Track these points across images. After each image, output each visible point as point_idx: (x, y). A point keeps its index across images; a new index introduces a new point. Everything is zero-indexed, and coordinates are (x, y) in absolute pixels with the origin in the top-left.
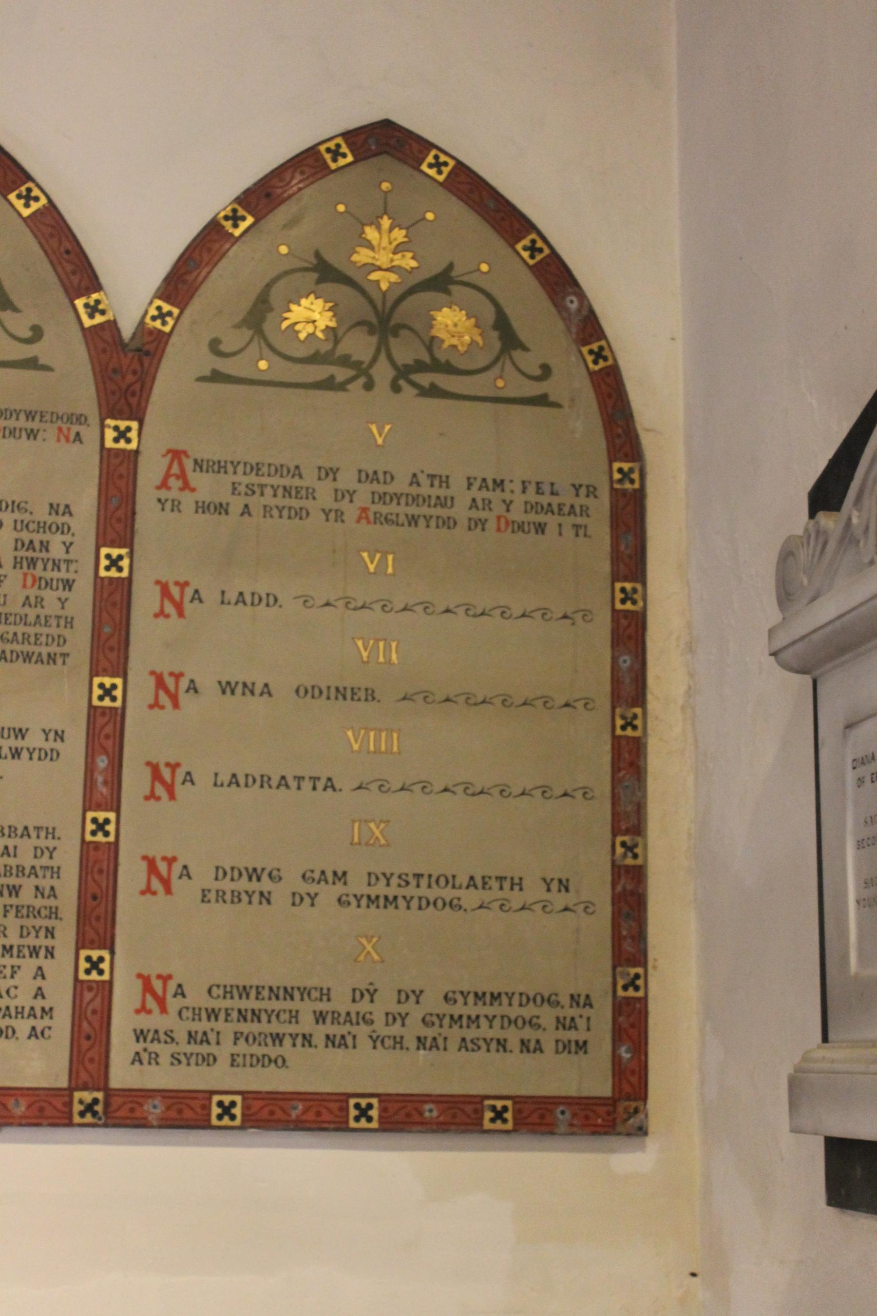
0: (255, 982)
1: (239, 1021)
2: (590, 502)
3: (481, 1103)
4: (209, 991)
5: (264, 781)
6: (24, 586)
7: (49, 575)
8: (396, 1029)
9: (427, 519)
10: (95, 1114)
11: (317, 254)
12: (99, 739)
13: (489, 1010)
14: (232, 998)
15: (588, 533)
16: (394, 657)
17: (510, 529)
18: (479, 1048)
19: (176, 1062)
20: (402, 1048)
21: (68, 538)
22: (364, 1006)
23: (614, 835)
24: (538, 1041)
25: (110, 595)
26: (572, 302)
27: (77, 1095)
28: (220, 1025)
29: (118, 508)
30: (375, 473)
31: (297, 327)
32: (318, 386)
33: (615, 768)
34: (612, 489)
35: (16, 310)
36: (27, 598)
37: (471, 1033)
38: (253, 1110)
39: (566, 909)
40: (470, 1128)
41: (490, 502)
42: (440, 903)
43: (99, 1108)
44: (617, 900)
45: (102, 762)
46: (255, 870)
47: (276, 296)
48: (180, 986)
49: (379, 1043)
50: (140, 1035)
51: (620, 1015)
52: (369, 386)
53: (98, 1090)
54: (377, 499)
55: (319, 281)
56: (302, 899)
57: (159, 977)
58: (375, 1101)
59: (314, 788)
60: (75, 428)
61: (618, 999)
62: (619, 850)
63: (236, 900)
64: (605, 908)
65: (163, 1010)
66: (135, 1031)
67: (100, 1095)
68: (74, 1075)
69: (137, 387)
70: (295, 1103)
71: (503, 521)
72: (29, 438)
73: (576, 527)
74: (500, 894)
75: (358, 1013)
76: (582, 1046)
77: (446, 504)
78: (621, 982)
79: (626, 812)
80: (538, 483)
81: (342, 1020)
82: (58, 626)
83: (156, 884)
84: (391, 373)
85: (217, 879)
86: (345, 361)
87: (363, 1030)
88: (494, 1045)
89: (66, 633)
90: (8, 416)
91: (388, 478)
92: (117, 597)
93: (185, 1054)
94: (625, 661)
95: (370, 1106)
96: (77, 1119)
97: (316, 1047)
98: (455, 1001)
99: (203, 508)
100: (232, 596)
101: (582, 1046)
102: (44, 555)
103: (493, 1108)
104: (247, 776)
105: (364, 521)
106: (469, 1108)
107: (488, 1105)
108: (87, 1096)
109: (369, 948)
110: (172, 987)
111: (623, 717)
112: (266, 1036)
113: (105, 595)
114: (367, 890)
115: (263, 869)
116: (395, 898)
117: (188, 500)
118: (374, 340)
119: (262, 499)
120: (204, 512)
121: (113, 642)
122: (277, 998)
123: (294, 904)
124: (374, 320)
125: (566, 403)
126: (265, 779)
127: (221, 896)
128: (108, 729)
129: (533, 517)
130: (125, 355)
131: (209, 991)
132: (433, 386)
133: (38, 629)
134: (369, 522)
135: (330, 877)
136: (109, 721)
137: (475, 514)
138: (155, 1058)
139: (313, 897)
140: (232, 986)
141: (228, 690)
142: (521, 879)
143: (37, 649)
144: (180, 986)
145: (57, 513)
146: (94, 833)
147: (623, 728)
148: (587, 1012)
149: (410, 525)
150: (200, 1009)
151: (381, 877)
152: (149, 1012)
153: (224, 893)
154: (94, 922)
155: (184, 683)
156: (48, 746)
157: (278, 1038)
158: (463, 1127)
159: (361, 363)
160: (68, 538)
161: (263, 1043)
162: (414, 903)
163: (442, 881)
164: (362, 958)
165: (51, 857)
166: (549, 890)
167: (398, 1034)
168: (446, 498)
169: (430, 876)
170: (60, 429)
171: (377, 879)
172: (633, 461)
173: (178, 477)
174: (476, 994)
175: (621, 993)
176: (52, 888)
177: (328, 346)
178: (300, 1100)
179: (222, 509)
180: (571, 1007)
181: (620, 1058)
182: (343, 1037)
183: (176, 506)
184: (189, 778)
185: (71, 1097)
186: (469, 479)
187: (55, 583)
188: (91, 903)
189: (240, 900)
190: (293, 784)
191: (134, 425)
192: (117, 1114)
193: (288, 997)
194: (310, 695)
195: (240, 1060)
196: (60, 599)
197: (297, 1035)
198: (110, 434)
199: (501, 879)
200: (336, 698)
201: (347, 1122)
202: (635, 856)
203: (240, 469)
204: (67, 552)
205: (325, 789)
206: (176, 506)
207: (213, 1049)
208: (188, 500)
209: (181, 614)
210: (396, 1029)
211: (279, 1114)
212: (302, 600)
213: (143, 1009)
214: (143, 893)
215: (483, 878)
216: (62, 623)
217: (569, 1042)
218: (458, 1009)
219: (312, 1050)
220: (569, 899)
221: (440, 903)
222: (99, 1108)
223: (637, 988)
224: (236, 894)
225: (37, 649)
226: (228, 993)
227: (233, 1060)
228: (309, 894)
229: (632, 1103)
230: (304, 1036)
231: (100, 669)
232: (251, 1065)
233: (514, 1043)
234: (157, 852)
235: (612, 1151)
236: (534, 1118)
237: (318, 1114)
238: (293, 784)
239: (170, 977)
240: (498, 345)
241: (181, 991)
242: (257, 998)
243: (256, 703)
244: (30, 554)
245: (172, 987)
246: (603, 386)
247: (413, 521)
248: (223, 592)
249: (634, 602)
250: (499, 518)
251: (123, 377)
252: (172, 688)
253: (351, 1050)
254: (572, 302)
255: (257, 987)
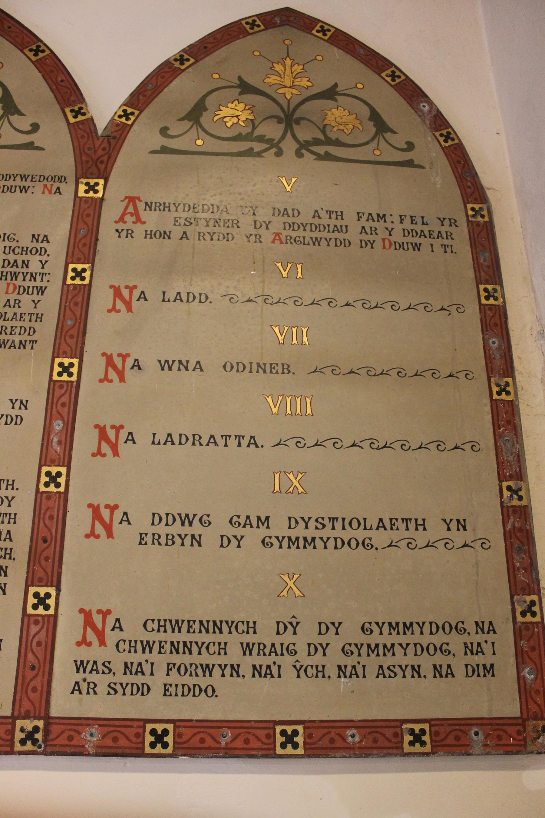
0: (187, 618)
1: (171, 652)
2: (453, 229)
3: (401, 726)
4: (145, 625)
5: (196, 439)
6: (7, 292)
7: (27, 284)
8: (318, 659)
9: (328, 241)
10: (35, 742)
11: (240, 78)
12: (56, 408)
13: (403, 639)
14: (165, 631)
15: (454, 250)
16: (305, 339)
17: (393, 247)
18: (396, 674)
19: (112, 692)
20: (324, 677)
21: (44, 258)
22: (288, 638)
23: (501, 481)
24: (449, 666)
25: (73, 297)
26: (424, 106)
27: (19, 723)
28: (154, 657)
29: (85, 237)
30: (286, 210)
31: (225, 120)
32: (240, 154)
33: (496, 426)
34: (468, 221)
35: (21, 114)
36: (8, 300)
37: (387, 661)
38: (185, 738)
39: (465, 545)
40: (391, 751)
41: (376, 229)
42: (353, 544)
43: (39, 736)
44: (508, 536)
45: (58, 426)
46: (187, 516)
47: (210, 101)
48: (118, 620)
49: (302, 673)
50: (80, 666)
51: (521, 640)
52: (279, 153)
53: (39, 718)
54: (287, 227)
55: (240, 94)
56: (229, 541)
57: (99, 612)
58: (300, 728)
59: (239, 445)
60: (56, 185)
61: (518, 625)
62: (506, 493)
63: (170, 542)
64: (499, 544)
65: (102, 642)
66: (76, 661)
67: (40, 724)
68: (17, 704)
69: (105, 158)
70: (225, 731)
71: (387, 242)
72: (21, 192)
73: (445, 246)
74: (406, 534)
75: (282, 644)
76: (489, 670)
77: (342, 231)
78: (519, 610)
79: (508, 462)
80: (411, 217)
81: (267, 651)
82: (30, 320)
83: (99, 529)
84: (296, 146)
85: (153, 524)
86: (261, 139)
87: (287, 661)
88: (409, 672)
89: (37, 326)
90: (8, 179)
91: (296, 213)
92: (79, 299)
93: (121, 684)
94: (494, 343)
95: (295, 733)
96: (18, 747)
97: (243, 676)
98: (372, 632)
99: (150, 235)
100: (171, 295)
101: (489, 670)
102: (25, 270)
103: (412, 732)
104: (180, 435)
105: (277, 242)
106: (389, 733)
107: (407, 728)
108: (29, 724)
109: (291, 584)
110: (110, 621)
111: (497, 385)
112: (197, 667)
113: (70, 297)
114: (288, 533)
115: (195, 515)
116: (314, 539)
117: (139, 230)
118: (283, 126)
119: (197, 228)
120: (151, 238)
121: (74, 332)
122: (207, 631)
123: (222, 546)
124: (282, 115)
125: (427, 166)
126: (197, 438)
127: (156, 538)
128: (64, 399)
129: (410, 239)
130: (98, 139)
131: (145, 625)
132: (327, 153)
133: (14, 323)
134: (281, 242)
135: (254, 522)
136: (66, 392)
137: (364, 237)
138: (93, 688)
139: (239, 540)
140: (165, 621)
141: (166, 366)
142: (424, 520)
143: (11, 338)
144: (118, 620)
145: (37, 241)
146: (47, 485)
147: (499, 393)
148: (491, 637)
149: (314, 244)
150: (136, 642)
151: (300, 520)
152: (89, 644)
153: (160, 536)
154: (43, 562)
155: (130, 362)
156: (13, 413)
157: (208, 669)
158: (385, 751)
159: (273, 140)
160: (44, 258)
161: (194, 674)
162: (331, 544)
163: (355, 524)
164: (284, 593)
165: (9, 506)
166: (449, 529)
167: (320, 664)
168: (341, 226)
169: (344, 519)
170: (45, 186)
171: (297, 522)
172: (482, 203)
173: (132, 215)
174: (390, 624)
175: (519, 619)
176: (9, 532)
177: (249, 130)
178: (229, 728)
179: (165, 235)
180: (477, 633)
181: (524, 677)
182: (268, 667)
183: (130, 234)
184: (131, 438)
185: (14, 725)
186: (358, 213)
187: (31, 289)
188: (42, 545)
189: (173, 543)
190: (221, 442)
191: (101, 182)
192: (55, 742)
193: (217, 631)
194: (235, 369)
195: (172, 690)
196: (33, 301)
197: (226, 666)
198: (82, 188)
199: (406, 521)
200: (258, 372)
201: (275, 749)
202: (520, 498)
203: (181, 208)
204: (43, 268)
205: (248, 446)
206: (130, 234)
207: (147, 679)
208: (139, 230)
209: (129, 309)
210: (318, 659)
211: (209, 742)
212: (228, 298)
213: (84, 642)
214: (87, 536)
215: (391, 520)
216: (34, 318)
217: (478, 665)
218: (375, 639)
219: (240, 680)
220: (467, 536)
221: (353, 544)
222: (39, 736)
223: (534, 614)
224: (170, 537)
225: (11, 338)
226: (161, 627)
227: (166, 690)
228: (235, 537)
229: (539, 722)
230: (232, 666)
231: (61, 351)
232: (183, 695)
233: (427, 669)
234: (101, 501)
235: (524, 768)
236: (451, 740)
237: (247, 741)
238: (221, 442)
239: (109, 612)
240: (374, 130)
241: (118, 626)
242: (188, 632)
243: (191, 377)
244: (14, 269)
245: (110, 621)
246: (453, 156)
247: (316, 242)
248: (164, 293)
249: (496, 299)
250: (384, 240)
251: (95, 152)
252: (120, 366)
253: (276, 679)
254: (424, 106)
255: (189, 621)
